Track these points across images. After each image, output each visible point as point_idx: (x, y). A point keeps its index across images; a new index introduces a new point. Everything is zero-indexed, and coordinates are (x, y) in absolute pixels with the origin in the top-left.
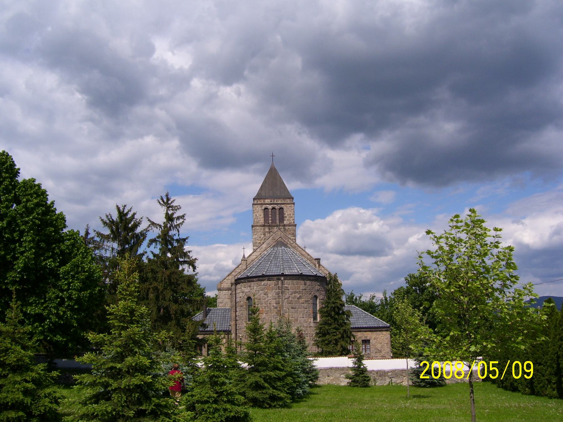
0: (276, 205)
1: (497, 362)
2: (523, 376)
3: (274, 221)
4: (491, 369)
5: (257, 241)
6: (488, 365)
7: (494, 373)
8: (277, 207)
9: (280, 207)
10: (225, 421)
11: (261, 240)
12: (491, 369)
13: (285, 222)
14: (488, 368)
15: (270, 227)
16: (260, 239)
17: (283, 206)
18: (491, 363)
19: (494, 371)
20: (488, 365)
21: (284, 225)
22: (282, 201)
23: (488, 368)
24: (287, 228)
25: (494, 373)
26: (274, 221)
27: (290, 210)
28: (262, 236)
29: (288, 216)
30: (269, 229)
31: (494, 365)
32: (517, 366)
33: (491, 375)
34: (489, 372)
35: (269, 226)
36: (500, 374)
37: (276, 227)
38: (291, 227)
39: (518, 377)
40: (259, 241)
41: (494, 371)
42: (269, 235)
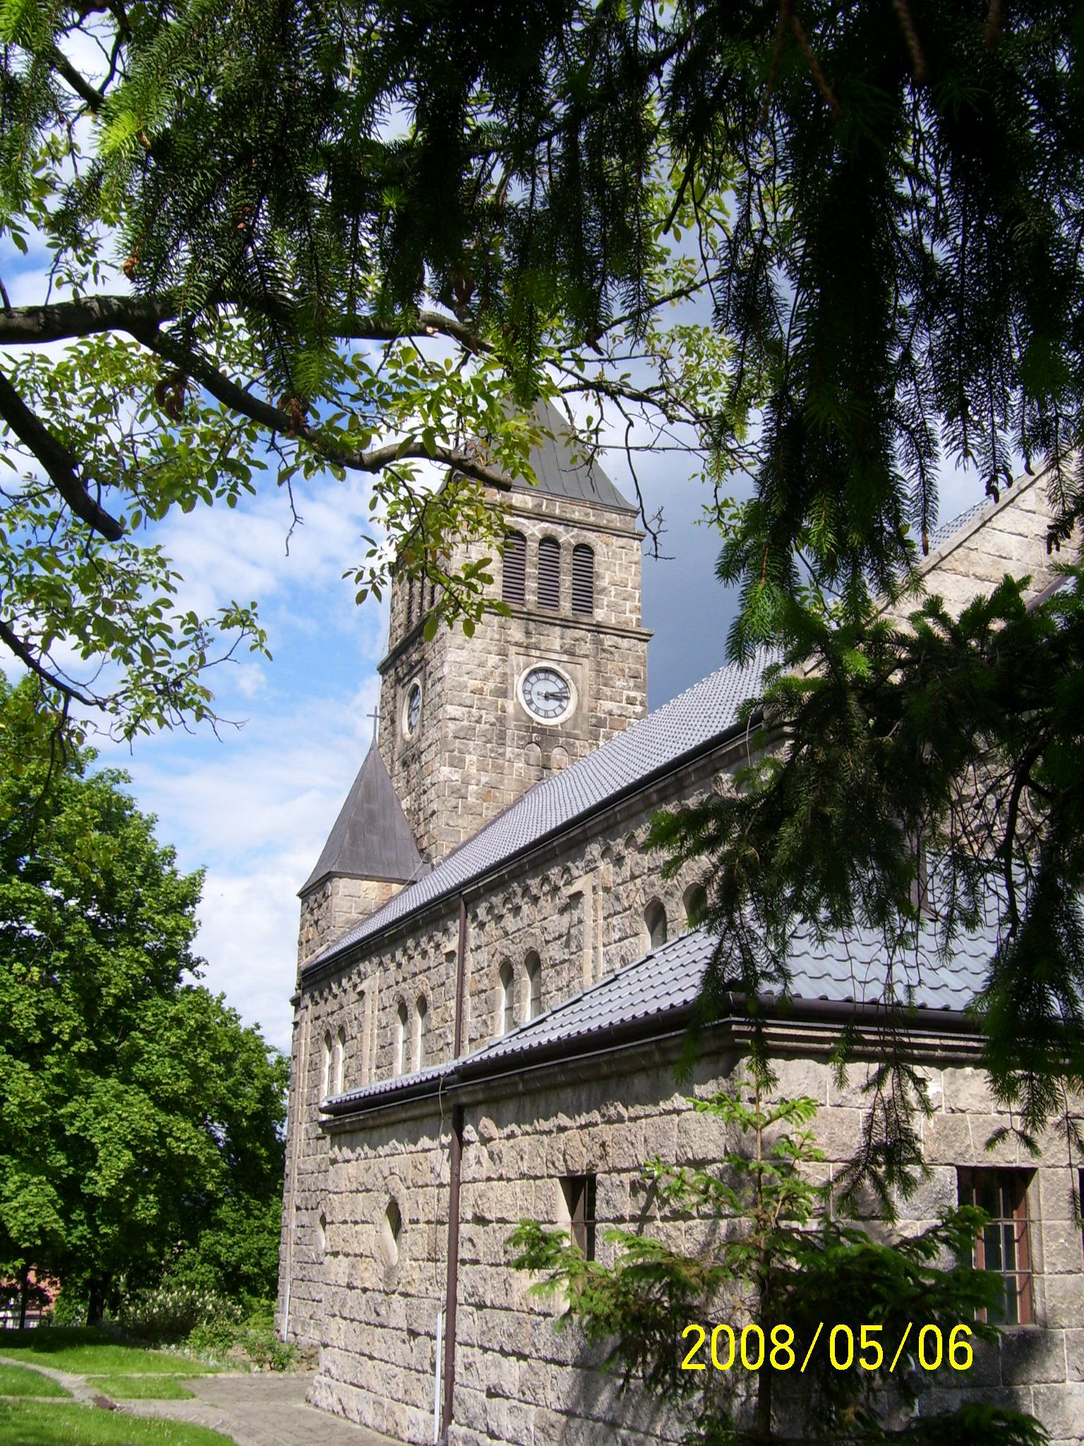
0: (561, 529)
1: (879, 1328)
2: (856, 1360)
3: (549, 595)
4: (865, 1344)
5: (466, 678)
6: (857, 1334)
7: (871, 1355)
8: (567, 537)
9: (581, 540)
10: (3, 1002)
11: (485, 679)
12: (865, 1344)
13: (600, 615)
14: (857, 1344)
15: (532, 625)
16: (481, 672)
17: (591, 538)
18: (864, 1329)
19: (873, 1349)
20: (857, 1334)
21: (598, 628)
22: (587, 515)
23: (857, 1344)
24: (608, 641)
25: (871, 1355)
26: (549, 595)
27: (624, 562)
28: (493, 659)
29: (612, 588)
30: (528, 633)
31: (872, 1337)
32: (842, 1336)
33: (863, 1361)
34: (859, 1352)
35: (528, 617)
36: (887, 1362)
37: (557, 630)
38: (625, 643)
39: (844, 1367)
40: (478, 684)
41: (873, 1349)
42: (522, 659)
